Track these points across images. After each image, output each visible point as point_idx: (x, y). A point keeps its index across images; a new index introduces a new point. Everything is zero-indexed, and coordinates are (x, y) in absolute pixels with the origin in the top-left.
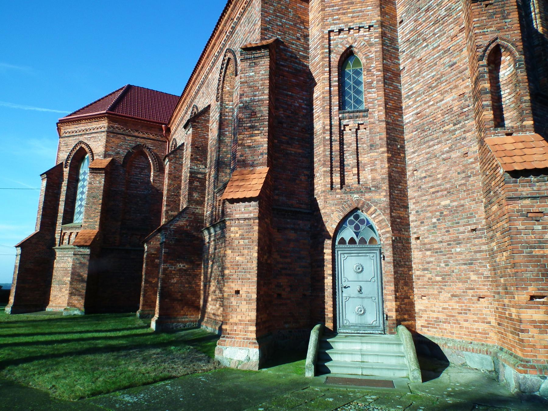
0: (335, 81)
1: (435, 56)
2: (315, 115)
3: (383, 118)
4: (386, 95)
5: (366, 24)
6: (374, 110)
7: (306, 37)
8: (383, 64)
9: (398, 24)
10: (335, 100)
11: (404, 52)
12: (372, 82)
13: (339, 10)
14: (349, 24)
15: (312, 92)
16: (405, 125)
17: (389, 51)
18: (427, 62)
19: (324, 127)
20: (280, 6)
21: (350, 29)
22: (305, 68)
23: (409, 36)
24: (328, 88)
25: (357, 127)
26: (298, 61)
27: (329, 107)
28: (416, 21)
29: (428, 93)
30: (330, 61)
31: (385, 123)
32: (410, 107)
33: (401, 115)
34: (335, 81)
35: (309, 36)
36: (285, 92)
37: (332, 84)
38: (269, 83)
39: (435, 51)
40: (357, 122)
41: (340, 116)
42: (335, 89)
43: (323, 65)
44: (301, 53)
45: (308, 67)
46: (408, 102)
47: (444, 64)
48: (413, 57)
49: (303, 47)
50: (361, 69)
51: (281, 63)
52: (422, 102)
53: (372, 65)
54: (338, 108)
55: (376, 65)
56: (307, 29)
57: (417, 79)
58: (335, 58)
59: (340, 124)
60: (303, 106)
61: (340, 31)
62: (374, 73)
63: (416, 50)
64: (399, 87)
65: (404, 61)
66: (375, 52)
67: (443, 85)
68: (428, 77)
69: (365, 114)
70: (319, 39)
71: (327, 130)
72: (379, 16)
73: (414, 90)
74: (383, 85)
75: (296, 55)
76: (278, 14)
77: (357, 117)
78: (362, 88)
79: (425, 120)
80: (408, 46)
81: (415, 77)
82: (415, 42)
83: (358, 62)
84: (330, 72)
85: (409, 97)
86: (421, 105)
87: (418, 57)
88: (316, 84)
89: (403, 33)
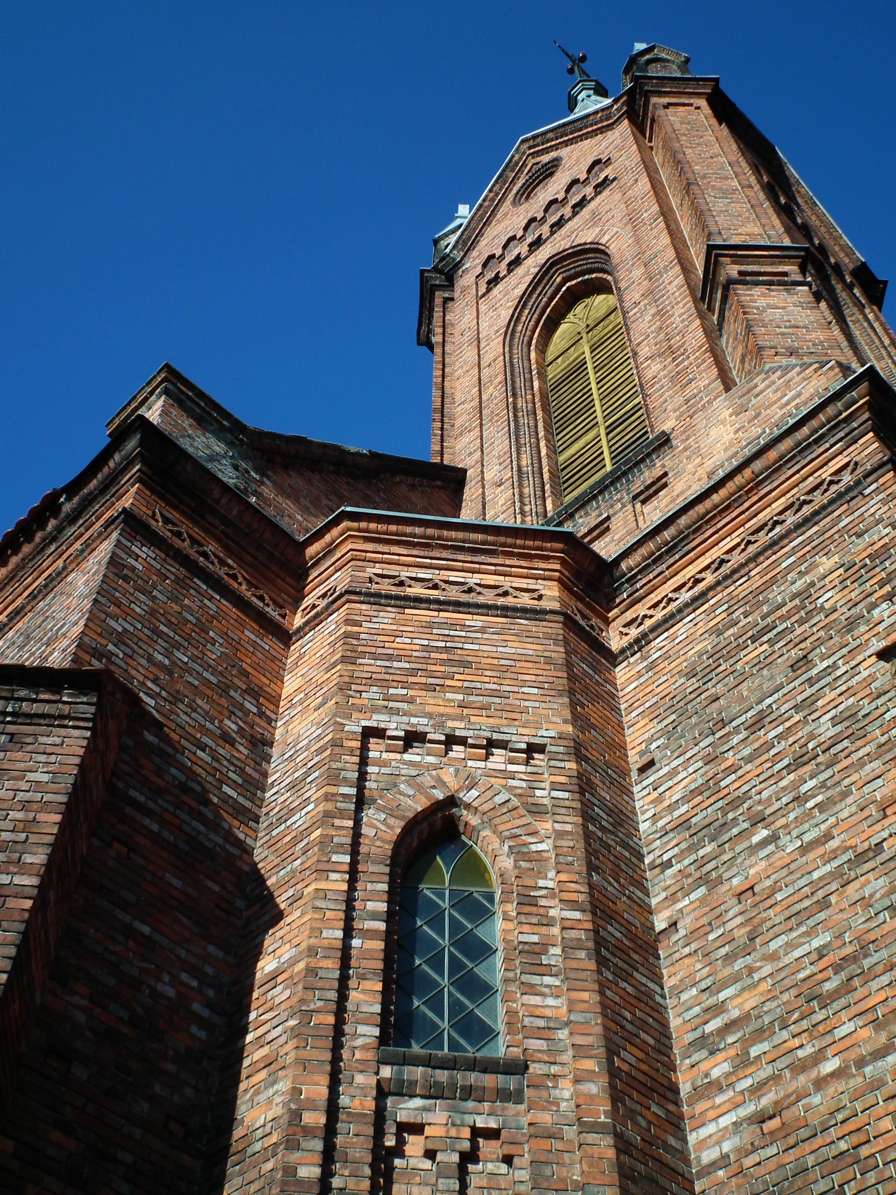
0: (374, 916)
1: (816, 875)
2: (253, 1056)
3: (602, 1113)
4: (608, 1010)
5: (520, 738)
6: (554, 1069)
7: (261, 745)
8: (591, 886)
9: (634, 775)
10: (366, 997)
11: (668, 864)
12: (543, 947)
13: (413, 672)
14: (450, 724)
15: (255, 953)
16: (700, 1175)
17: (608, 847)
18: (779, 896)
19: (296, 1115)
20: (177, 608)
21: (451, 740)
22: (236, 851)
23: (684, 809)
24: (340, 934)
25: (466, 1145)
26: (210, 816)
27: (331, 1019)
28: (709, 761)
29: (805, 1024)
30: (357, 834)
31: (609, 1140)
32: (717, 1086)
33: (676, 1124)
34: (374, 916)
35: (271, 744)
36: (121, 914)
37: (357, 924)
38: (62, 825)
39: (811, 856)
40: (469, 1119)
41: (386, 1072)
42: (369, 948)
43: (324, 842)
44: (226, 789)
45: (249, 852)
46: (704, 1066)
47: (865, 902)
48: (711, 882)
49: (241, 772)
50: (490, 897)
51: (133, 793)
52: (781, 1064)
53: (541, 883)
54: (376, 1032)
55: (560, 888)
56: (269, 721)
57: (739, 964)
58: (381, 829)
59: (380, 1116)
60: (196, 1007)
61: (412, 739)
62: (552, 913)
63: (725, 857)
64: (658, 998)
65: (672, 898)
66: (554, 835)
67: (874, 985)
68: (797, 953)
69: (512, 1082)
70: (320, 751)
71: (308, 1131)
72: (565, 722)
73: (735, 1014)
74: (592, 965)
75: (206, 791)
76: (162, 628)
77: (468, 1093)
78: (492, 970)
79: (807, 1147)
80: (683, 846)
81: (729, 958)
82: (716, 830)
83: (474, 869)
84: (353, 873)
85: (707, 1044)
86: (775, 1078)
87: (735, 881)
88: (279, 916)
89: (659, 800)
